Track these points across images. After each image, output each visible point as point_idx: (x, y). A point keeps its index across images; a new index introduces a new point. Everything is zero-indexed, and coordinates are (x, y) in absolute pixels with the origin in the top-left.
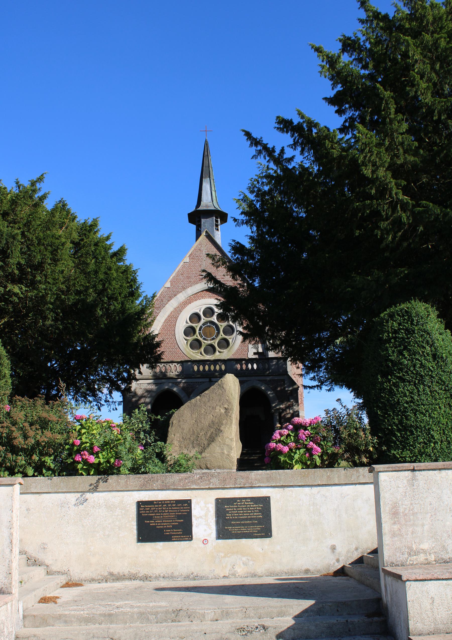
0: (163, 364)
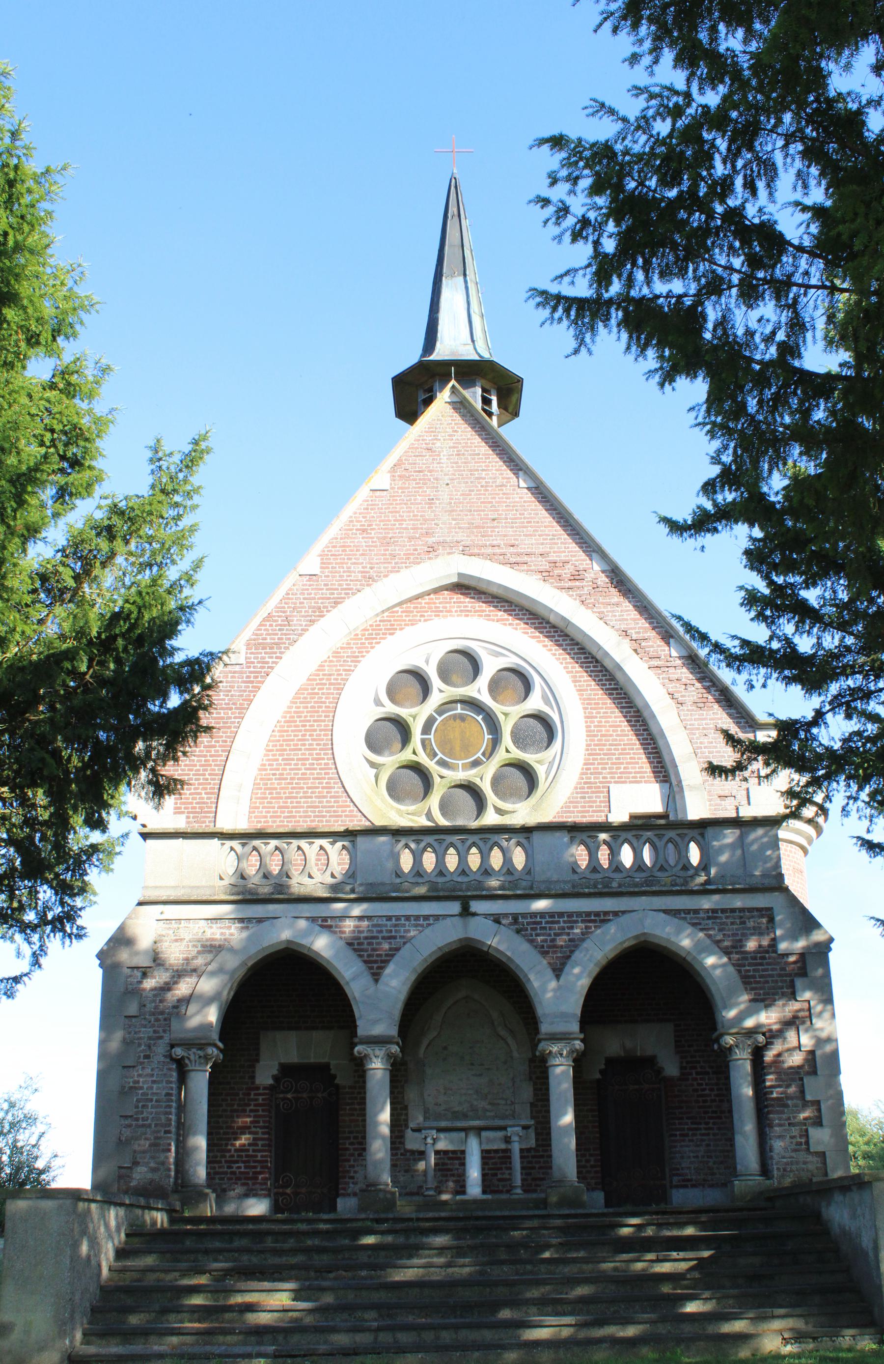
0: (274, 843)
